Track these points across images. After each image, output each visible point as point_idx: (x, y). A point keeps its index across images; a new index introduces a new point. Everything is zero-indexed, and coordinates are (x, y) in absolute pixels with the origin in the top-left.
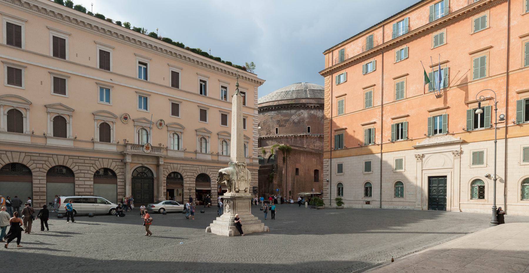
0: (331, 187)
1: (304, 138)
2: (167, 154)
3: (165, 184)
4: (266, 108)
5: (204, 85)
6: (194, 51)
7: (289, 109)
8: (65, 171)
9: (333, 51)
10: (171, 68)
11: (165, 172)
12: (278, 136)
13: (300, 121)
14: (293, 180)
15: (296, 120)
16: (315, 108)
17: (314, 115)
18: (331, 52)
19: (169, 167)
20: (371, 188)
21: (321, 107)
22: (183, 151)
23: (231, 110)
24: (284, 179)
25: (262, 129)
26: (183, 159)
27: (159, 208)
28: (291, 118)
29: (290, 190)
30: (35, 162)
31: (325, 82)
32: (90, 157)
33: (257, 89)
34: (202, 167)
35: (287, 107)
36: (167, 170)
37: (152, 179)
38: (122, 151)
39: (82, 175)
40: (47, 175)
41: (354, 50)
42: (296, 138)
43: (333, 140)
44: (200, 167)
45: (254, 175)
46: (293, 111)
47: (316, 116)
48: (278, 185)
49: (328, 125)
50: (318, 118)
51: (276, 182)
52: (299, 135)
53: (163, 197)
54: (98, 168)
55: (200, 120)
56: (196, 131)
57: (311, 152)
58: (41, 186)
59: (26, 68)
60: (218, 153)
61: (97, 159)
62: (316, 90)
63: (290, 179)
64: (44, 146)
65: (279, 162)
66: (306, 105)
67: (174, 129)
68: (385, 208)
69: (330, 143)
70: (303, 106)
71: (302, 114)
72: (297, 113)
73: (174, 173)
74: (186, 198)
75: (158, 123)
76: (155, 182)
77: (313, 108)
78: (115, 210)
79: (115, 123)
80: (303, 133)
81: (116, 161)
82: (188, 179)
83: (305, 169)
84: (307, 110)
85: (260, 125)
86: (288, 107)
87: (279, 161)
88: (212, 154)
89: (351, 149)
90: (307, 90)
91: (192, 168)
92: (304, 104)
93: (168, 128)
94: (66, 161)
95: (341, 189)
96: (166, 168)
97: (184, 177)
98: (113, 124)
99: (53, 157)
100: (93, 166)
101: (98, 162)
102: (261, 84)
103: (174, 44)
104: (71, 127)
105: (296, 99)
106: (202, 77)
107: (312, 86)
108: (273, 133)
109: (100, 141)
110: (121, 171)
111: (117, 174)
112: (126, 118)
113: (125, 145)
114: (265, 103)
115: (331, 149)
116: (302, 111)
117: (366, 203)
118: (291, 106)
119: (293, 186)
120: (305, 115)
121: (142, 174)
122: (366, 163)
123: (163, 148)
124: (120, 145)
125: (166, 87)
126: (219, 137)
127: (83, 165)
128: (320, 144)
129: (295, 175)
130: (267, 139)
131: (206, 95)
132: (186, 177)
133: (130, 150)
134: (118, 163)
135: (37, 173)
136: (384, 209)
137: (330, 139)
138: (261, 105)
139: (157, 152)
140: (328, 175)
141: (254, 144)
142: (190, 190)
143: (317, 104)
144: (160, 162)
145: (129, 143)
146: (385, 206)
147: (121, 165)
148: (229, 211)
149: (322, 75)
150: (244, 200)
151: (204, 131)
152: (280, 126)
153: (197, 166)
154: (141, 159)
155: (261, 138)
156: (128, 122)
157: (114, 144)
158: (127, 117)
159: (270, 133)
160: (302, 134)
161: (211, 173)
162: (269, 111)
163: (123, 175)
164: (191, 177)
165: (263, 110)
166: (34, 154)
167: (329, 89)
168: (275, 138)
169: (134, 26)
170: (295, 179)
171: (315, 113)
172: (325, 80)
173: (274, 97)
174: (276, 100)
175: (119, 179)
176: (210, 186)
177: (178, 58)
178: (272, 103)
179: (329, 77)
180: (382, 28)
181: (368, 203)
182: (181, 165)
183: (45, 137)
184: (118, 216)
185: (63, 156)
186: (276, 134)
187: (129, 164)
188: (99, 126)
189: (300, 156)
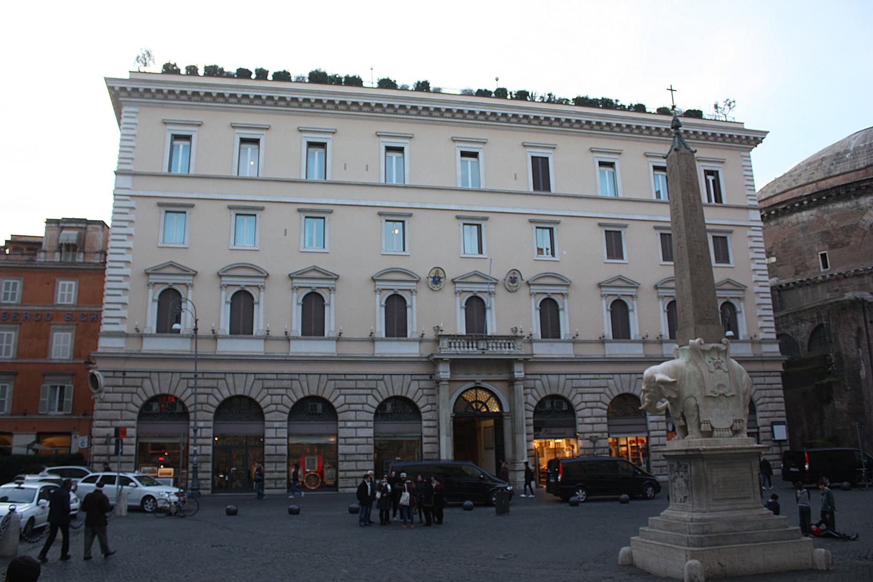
2: (532, 351)
4: (783, 206)
5: (713, 181)
8: (321, 407)
11: (530, 397)
22: (654, 342)
28: (861, 218)
30: (270, 391)
32: (367, 375)
34: (622, 376)
35: (847, 192)
36: (535, 393)
38: (429, 354)
39: (352, 415)
40: (289, 417)
44: (616, 376)
45: (769, 386)
54: (382, 397)
55: (608, 258)
58: (279, 443)
59: (331, 212)
60: (531, 335)
61: (381, 377)
64: (286, 357)
65: (842, 346)
78: (147, 501)
79: (416, 292)
82: (587, 412)
85: (773, 254)
86: (850, 191)
87: (845, 343)
91: (595, 383)
94: (322, 386)
96: (286, 389)
99: (301, 379)
100: (288, 394)
101: (149, 382)
110: (429, 402)
111: (422, 410)
113: (438, 339)
114: (780, 194)
123: (522, 337)
124: (427, 340)
127: (354, 391)
130: (800, 287)
131: (721, 202)
133: (448, 351)
134: (423, 384)
135: (272, 414)
138: (770, 201)
139: (508, 349)
144: (516, 374)
145: (444, 333)
148: (685, 497)
153: (607, 376)
157: (414, 340)
158: (516, 278)
161: (574, 391)
162: (795, 212)
163: (435, 411)
164: (594, 404)
165: (777, 211)
166: (268, 376)
168: (821, 282)
174: (811, 180)
178: (799, 192)
182: (568, 377)
183: (288, 339)
184: (770, 500)
185: (318, 376)
186: (822, 270)
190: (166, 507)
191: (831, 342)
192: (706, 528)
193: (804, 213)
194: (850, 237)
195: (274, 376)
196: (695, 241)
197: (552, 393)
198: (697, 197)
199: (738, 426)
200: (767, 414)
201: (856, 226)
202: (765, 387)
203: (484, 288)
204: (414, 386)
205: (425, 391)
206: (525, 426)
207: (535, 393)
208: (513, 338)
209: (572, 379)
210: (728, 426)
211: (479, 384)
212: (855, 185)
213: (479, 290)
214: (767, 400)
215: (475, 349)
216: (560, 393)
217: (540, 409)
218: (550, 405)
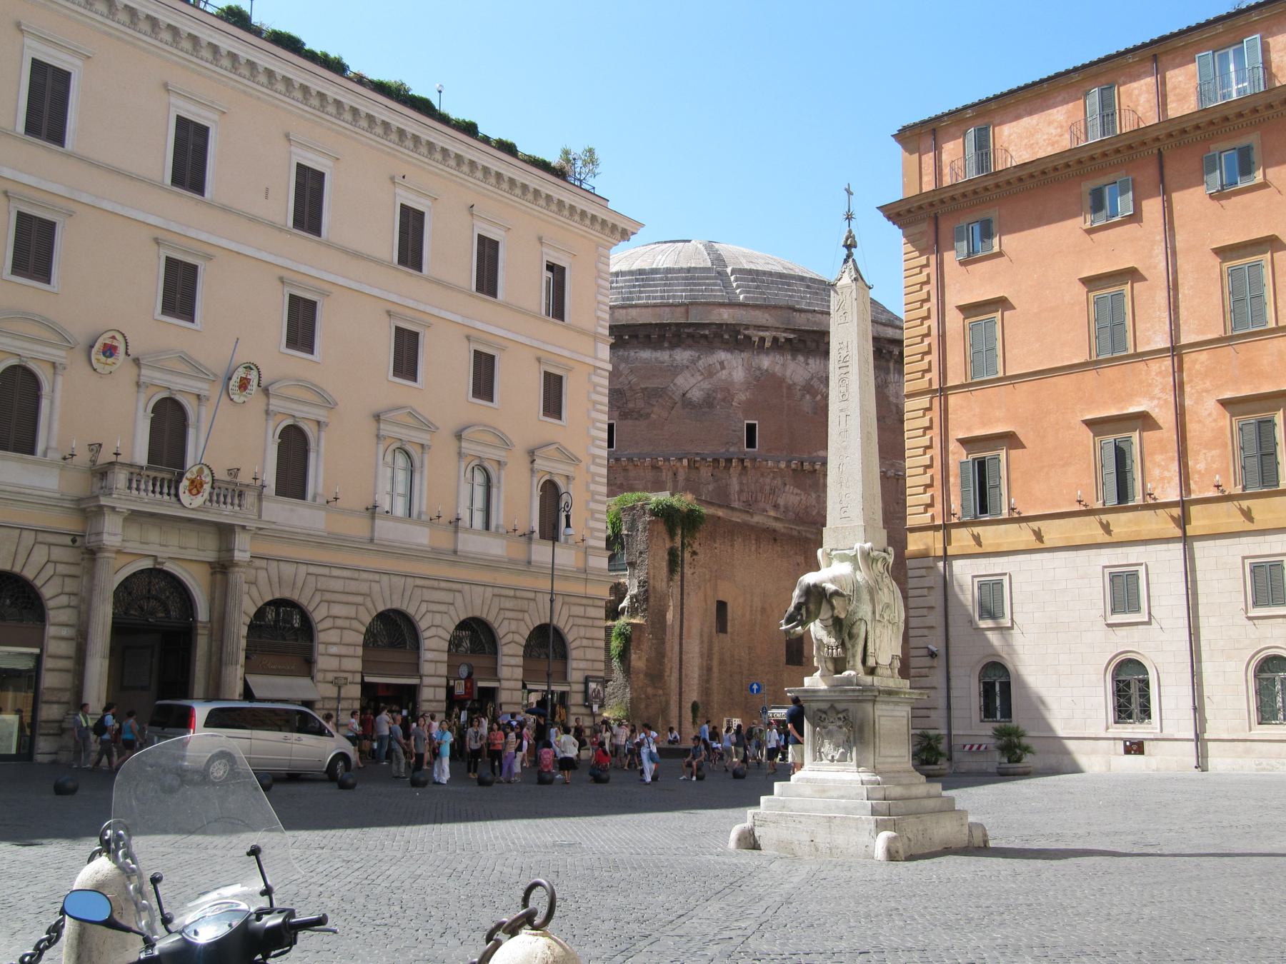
0: (948, 679)
6: (381, 88)
7: (666, 345)
13: (715, 398)
14: (707, 655)
15: (696, 395)
17: (774, 375)
23: (897, 337)
26: (321, 543)
29: (695, 699)
34: (394, 579)
41: (1032, 135)
42: (697, 468)
44: (385, 578)
45: (590, 622)
46: (682, 356)
47: (781, 380)
48: (647, 675)
50: (790, 387)
51: (640, 658)
54: (473, 611)
57: (775, 531)
67: (294, 406)
70: (726, 336)
71: (723, 368)
72: (700, 362)
73: (278, 603)
75: (234, 378)
81: (51, 538)
83: (751, 606)
84: (745, 355)
88: (434, 520)
91: (353, 586)
92: (734, 329)
95: (997, 688)
98: (55, 374)
102: (625, 235)
103: (312, 56)
104: (425, 483)
111: (51, 604)
112: (109, 351)
116: (723, 355)
117: (1128, 751)
119: (708, 681)
120: (735, 374)
125: (272, 225)
128: (798, 498)
129: (714, 630)
134: (57, 553)
139: (229, 507)
140: (932, 627)
143: (786, 330)
145: (120, 459)
147: (71, 561)
150: (897, 708)
153: (371, 576)
154: (154, 536)
156: (113, 368)
161: (424, 607)
164: (345, 623)
170: (716, 649)
171: (777, 369)
175: (54, 625)
176: (415, 669)
177: (327, 113)
181: (1135, 747)
182: (312, 569)
187: (114, 555)
189: (732, 546)
194: (653, 405)
195: (511, 593)
197: (282, 597)
201: (664, 390)
202: (583, 622)
204: (40, 555)
205: (61, 569)
209: (317, 575)
211: (163, 563)
214: (585, 642)
217: (257, 626)
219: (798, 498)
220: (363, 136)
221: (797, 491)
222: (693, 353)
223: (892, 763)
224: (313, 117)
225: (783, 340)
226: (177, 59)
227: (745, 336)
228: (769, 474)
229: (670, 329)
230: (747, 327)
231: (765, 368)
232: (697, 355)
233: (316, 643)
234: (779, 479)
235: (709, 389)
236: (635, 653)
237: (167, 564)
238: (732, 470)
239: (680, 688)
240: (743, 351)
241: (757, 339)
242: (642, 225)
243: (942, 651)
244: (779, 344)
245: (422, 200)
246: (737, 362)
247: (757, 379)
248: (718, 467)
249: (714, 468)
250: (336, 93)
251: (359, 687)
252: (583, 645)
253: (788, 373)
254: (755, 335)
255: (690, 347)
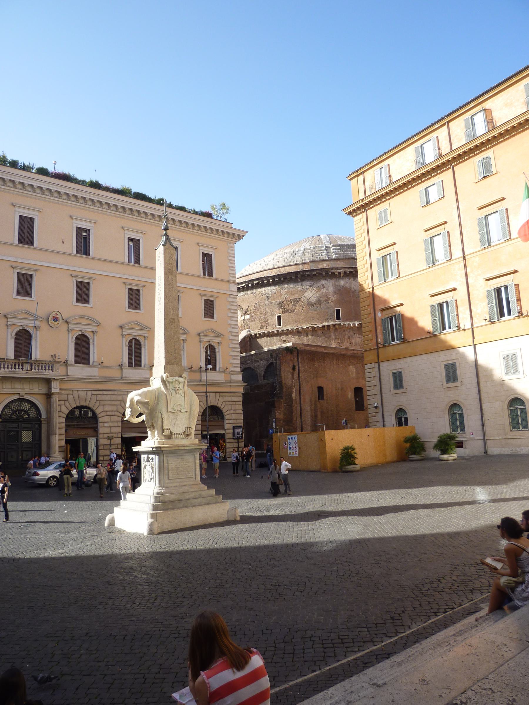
0: (383, 418)
1: (331, 330)
3: (63, 431)
7: (299, 280)
9: (363, 172)
10: (77, 222)
12: (283, 330)
15: (313, 300)
16: (346, 275)
17: (346, 288)
18: (360, 174)
19: (70, 397)
20: (461, 415)
21: (353, 273)
23: (234, 266)
24: (296, 408)
25: (252, 319)
27: (47, 478)
31: (355, 227)
33: (234, 248)
36: (67, 404)
37: (38, 420)
42: (316, 331)
43: (379, 328)
45: (234, 403)
47: (350, 289)
49: (369, 301)
50: (353, 292)
52: (320, 326)
53: (58, 455)
56: (121, 327)
60: (201, 368)
62: (346, 245)
63: (307, 409)
65: (283, 377)
66: (330, 272)
67: (21, 321)
68: (495, 453)
69: (375, 334)
71: (324, 287)
73: (80, 408)
74: (103, 456)
76: (44, 427)
77: (342, 275)
80: (328, 322)
84: (333, 281)
85: (248, 313)
86: (298, 277)
87: (285, 375)
89: (414, 342)
90: (331, 246)
91: (114, 398)
92: (327, 270)
93: (70, 325)
97: (99, 416)
104: (147, 352)
105: (310, 262)
106: (132, 234)
107: (339, 239)
108: (273, 324)
109: (75, 363)
112: (55, 319)
115: (377, 346)
118: (303, 276)
121: (20, 413)
122: (447, 366)
126: (124, 333)
128: (360, 339)
129: (317, 399)
132: (103, 414)
136: (493, 456)
137: (374, 327)
139: (47, 371)
141: (232, 346)
142: (109, 438)
146: (493, 450)
149: (348, 214)
151: (27, 316)
152: (284, 312)
155: (251, 335)
158: (58, 318)
159: (267, 325)
160: (326, 324)
164: (112, 413)
165: (253, 284)
167: (363, 236)
169: (170, 203)
171: (347, 285)
172: (355, 223)
173: (272, 262)
174: (276, 266)
177: (88, 205)
179: (361, 215)
180: (445, 127)
182: (94, 393)
186: (277, 327)
188: (127, 343)
189: (324, 363)
190: (521, 526)
191: (277, 374)
192: (161, 499)
193: (269, 288)
196: (170, 308)
198: (174, 279)
199: (188, 432)
200: (231, 421)
202: (231, 403)
203: (31, 323)
206: (58, 429)
207: (67, 404)
208: (50, 365)
210: (182, 431)
212: (301, 273)
213: (26, 324)
214: (232, 412)
215: (21, 370)
216: (87, 405)
218: (78, 413)
219: (360, 339)
220: (107, 212)
221: (360, 336)
222: (311, 282)
223: (180, 482)
224: (82, 207)
225: (349, 273)
226: (17, 193)
227: (332, 272)
228: (347, 330)
229: (300, 273)
230: (332, 269)
231: (342, 285)
232: (312, 283)
233: (99, 423)
234: (352, 332)
235: (319, 297)
236: (278, 412)
237: (25, 396)
238: (331, 330)
239: (302, 425)
240: (332, 279)
241: (337, 273)
242: (247, 232)
243: (380, 405)
244: (347, 274)
245: (138, 235)
246: (330, 284)
247: (339, 290)
248: (325, 329)
249: (323, 330)
250: (90, 196)
251: (120, 439)
252: (231, 413)
253: (352, 286)
254: (336, 272)
255: (309, 280)
